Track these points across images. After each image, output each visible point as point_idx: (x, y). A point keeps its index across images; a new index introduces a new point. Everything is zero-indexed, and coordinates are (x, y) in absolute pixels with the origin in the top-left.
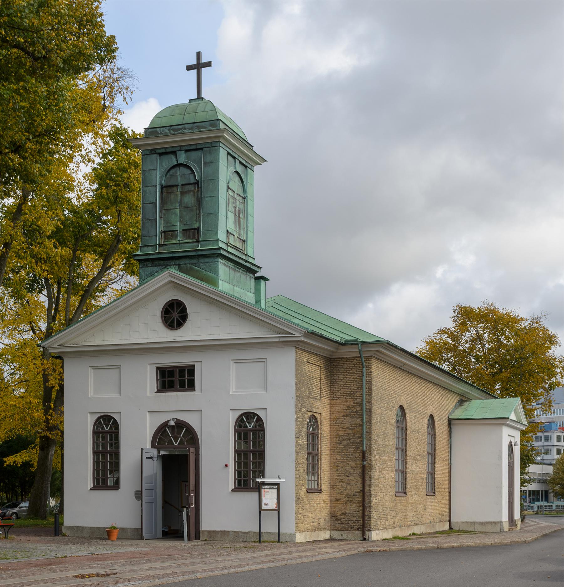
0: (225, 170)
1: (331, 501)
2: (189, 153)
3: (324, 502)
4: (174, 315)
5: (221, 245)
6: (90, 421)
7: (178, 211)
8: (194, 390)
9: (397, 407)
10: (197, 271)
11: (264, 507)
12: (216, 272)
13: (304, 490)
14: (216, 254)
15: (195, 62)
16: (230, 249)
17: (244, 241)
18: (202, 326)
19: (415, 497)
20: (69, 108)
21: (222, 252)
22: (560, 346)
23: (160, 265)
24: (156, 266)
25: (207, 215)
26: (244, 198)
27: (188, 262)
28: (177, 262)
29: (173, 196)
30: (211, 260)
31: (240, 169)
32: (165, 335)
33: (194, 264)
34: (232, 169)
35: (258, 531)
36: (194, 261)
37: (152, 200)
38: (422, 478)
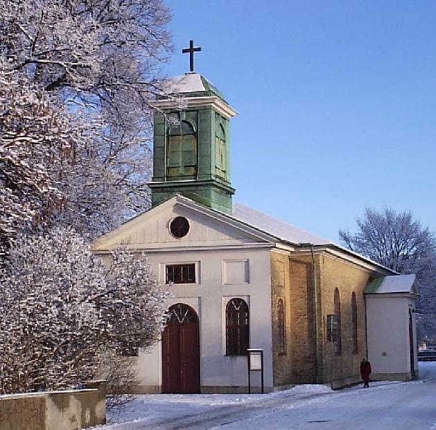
0: (214, 125)
1: (292, 362)
2: (188, 113)
3: (288, 362)
4: (179, 228)
5: (213, 178)
6: (225, 301)
7: (181, 153)
8: (194, 281)
9: (334, 289)
10: (195, 195)
11: (251, 368)
12: (209, 196)
13: (277, 354)
14: (210, 183)
15: (189, 48)
16: (217, 180)
17: (225, 172)
18: (199, 233)
19: (347, 356)
20: (396, 225)
21: (214, 183)
22: (228, 121)
23: (167, 191)
24: (164, 192)
25: (203, 156)
26: (224, 141)
27: (188, 189)
28: (181, 189)
29: (177, 143)
30: (206, 188)
31: (221, 121)
32: (175, 243)
33: (194, 191)
34: (218, 123)
35: (248, 385)
36: (194, 188)
37: (161, 144)
38: (350, 341)
